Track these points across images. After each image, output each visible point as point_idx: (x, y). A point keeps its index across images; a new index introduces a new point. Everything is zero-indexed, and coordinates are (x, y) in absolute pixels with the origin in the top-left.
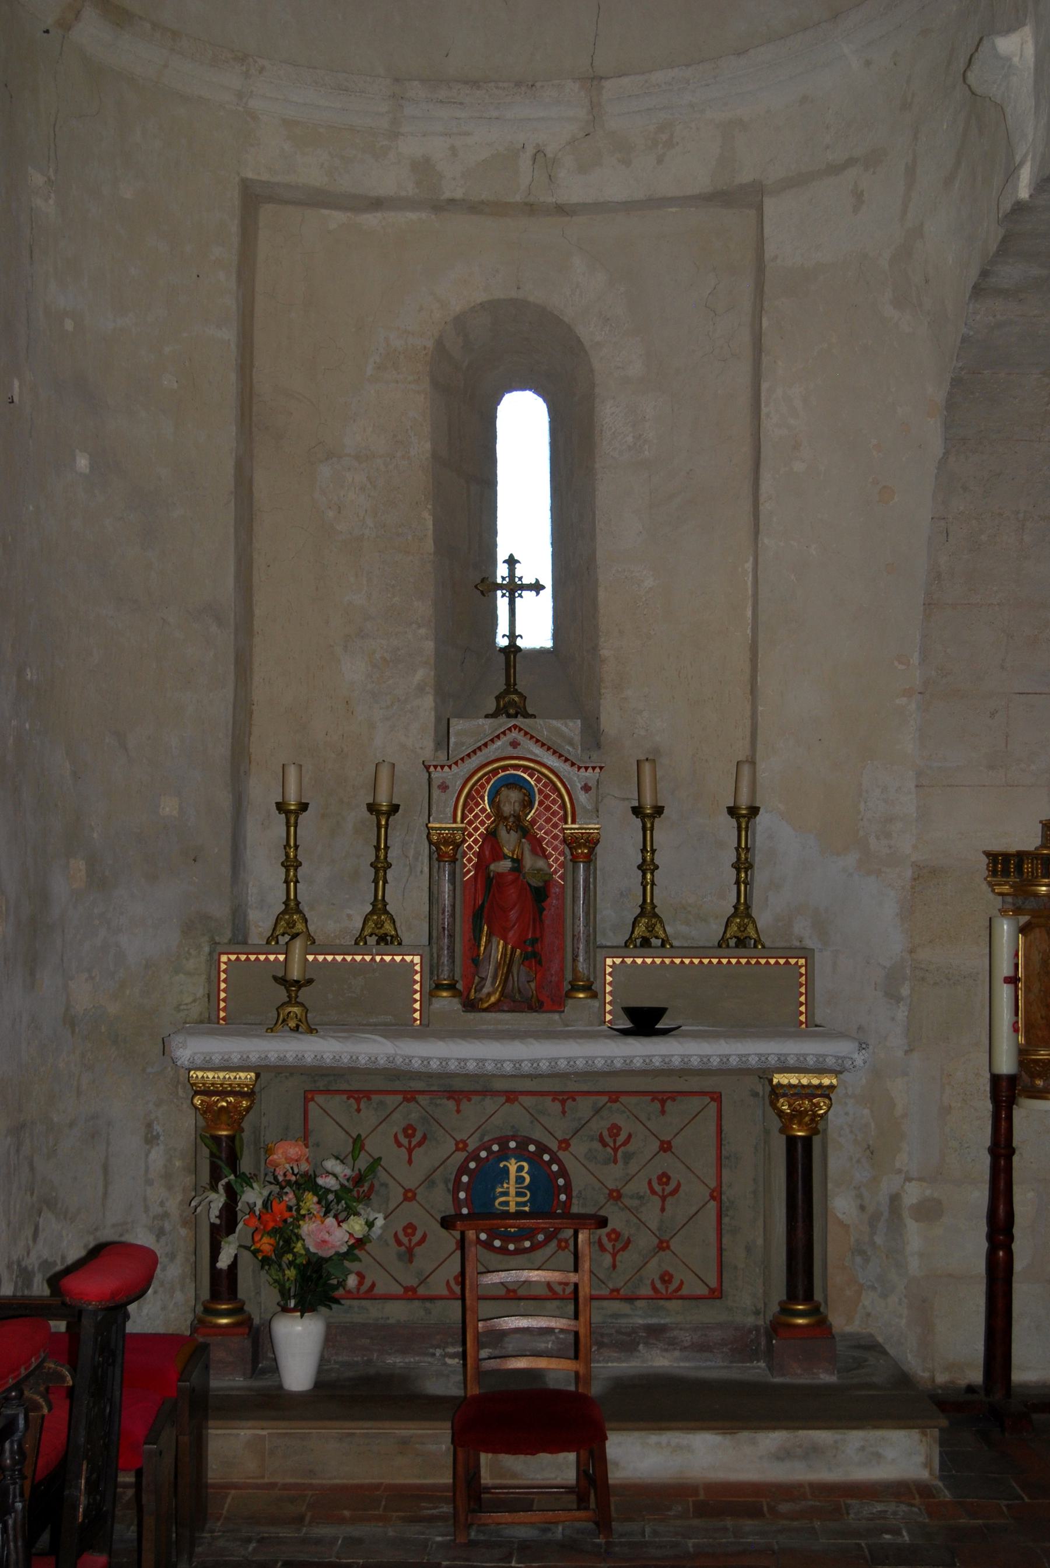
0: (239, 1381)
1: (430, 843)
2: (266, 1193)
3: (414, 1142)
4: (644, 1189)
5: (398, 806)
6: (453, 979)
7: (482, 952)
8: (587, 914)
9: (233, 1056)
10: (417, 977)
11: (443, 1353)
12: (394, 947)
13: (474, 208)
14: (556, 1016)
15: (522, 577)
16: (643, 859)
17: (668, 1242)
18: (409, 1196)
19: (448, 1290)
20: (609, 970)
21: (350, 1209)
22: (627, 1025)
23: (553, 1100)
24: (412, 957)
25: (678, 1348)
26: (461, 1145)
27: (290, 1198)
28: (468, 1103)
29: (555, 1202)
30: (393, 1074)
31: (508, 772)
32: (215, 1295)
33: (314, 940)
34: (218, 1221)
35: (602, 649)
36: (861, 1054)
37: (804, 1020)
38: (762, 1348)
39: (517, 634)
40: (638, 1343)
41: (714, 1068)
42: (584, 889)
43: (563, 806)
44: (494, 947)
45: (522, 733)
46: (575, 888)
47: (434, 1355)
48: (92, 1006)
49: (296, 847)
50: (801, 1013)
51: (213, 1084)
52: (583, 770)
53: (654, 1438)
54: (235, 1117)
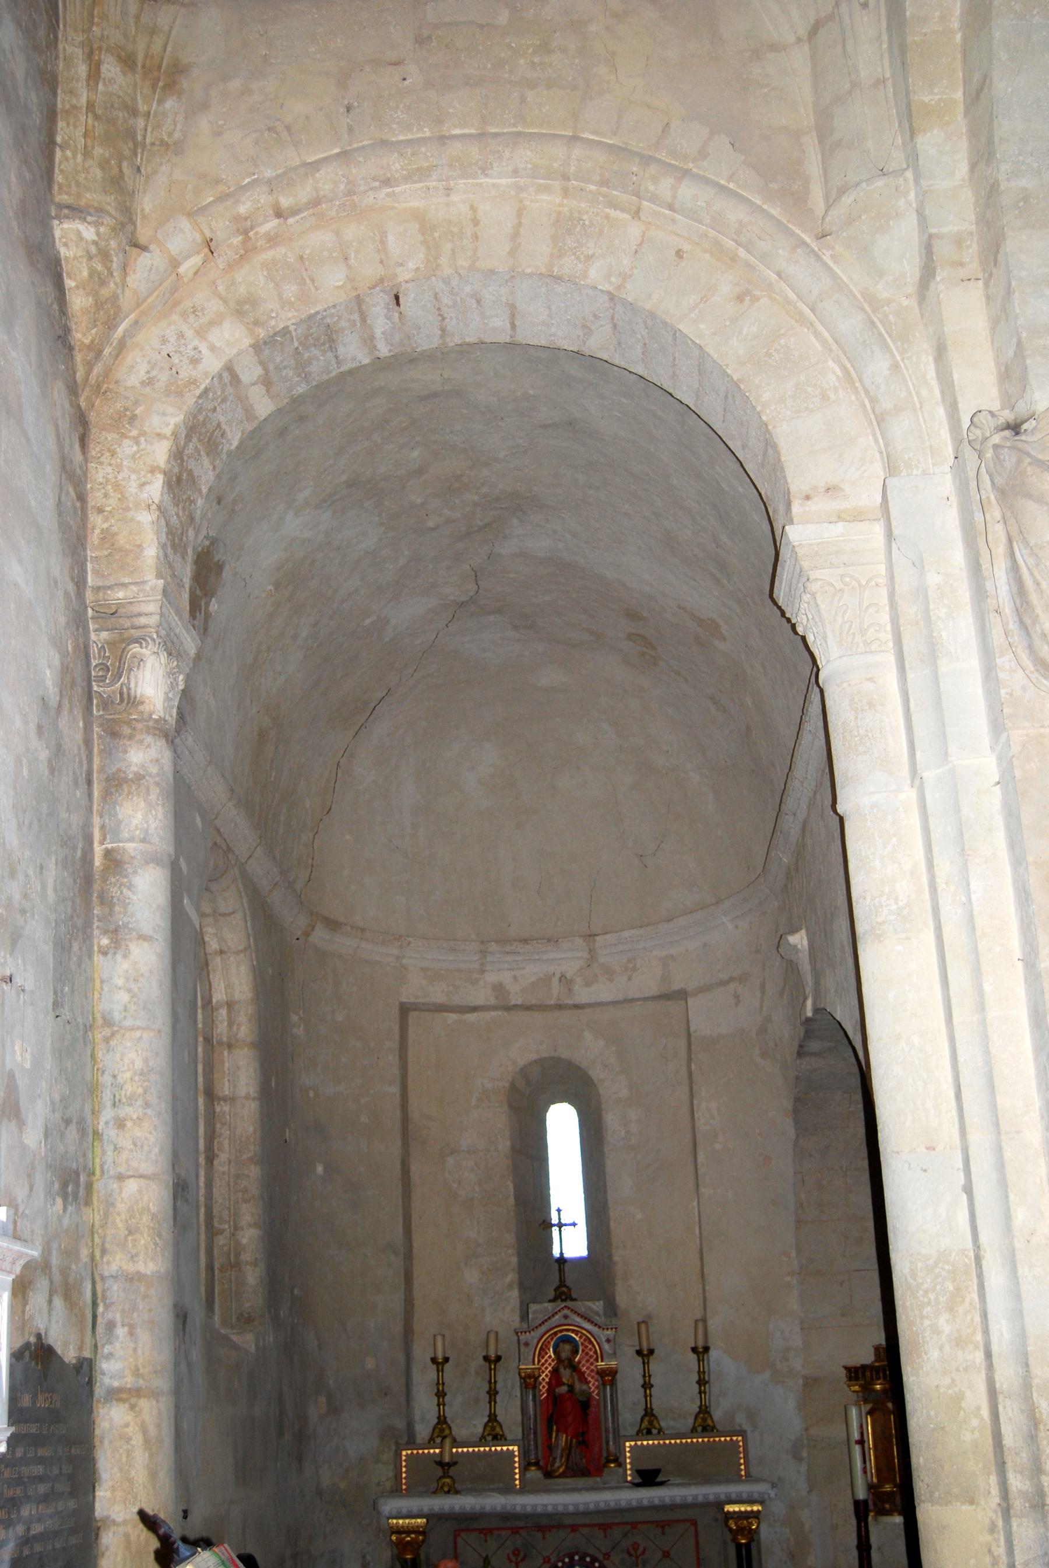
1: (521, 1377)
3: (520, 1558)
12: (503, 1442)
13: (528, 1008)
14: (598, 1479)
20: (628, 1449)
22: (638, 1480)
30: (506, 1517)
43: (595, 1352)
49: (443, 1384)
54: (415, 1546)
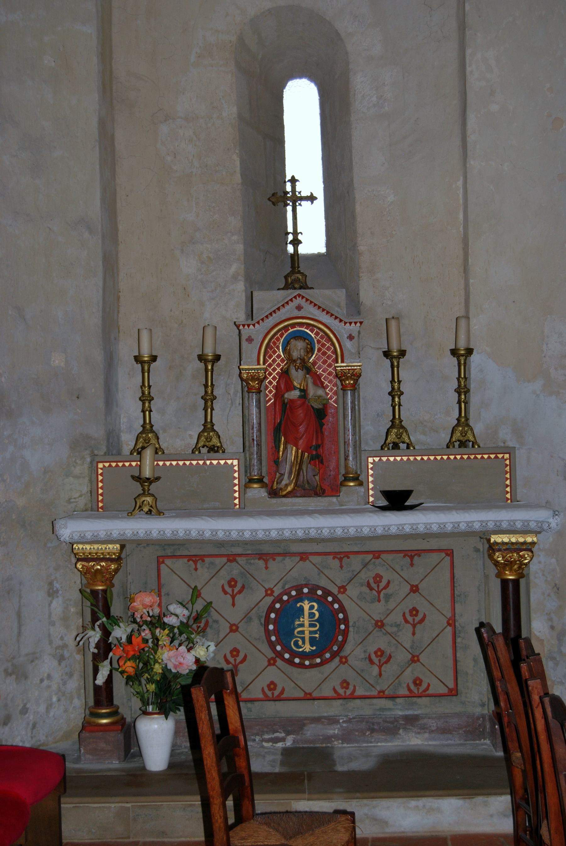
0: (115, 763)
1: (242, 380)
2: (129, 630)
3: (236, 590)
4: (400, 619)
5: (220, 356)
6: (261, 475)
7: (281, 455)
8: (354, 427)
9: (126, 532)
10: (236, 475)
11: (261, 739)
14: (334, 499)
15: (301, 192)
16: (392, 388)
17: (418, 656)
18: (234, 628)
19: (263, 694)
20: (370, 466)
21: (190, 639)
22: (383, 502)
23: (334, 558)
24: (232, 461)
25: (427, 731)
26: (269, 592)
27: (146, 633)
28: (273, 562)
29: (337, 630)
31: (295, 329)
32: (98, 703)
33: (164, 451)
34: (96, 651)
35: (359, 246)
36: (554, 518)
37: (509, 497)
38: (488, 730)
39: (298, 232)
40: (399, 729)
41: (448, 532)
42: (352, 410)
43: (335, 352)
44: (289, 452)
45: (304, 300)
46: (345, 409)
47: (254, 740)
48: (4, 500)
49: (150, 387)
50: (507, 492)
51: (90, 553)
52: (348, 324)
53: (413, 803)
